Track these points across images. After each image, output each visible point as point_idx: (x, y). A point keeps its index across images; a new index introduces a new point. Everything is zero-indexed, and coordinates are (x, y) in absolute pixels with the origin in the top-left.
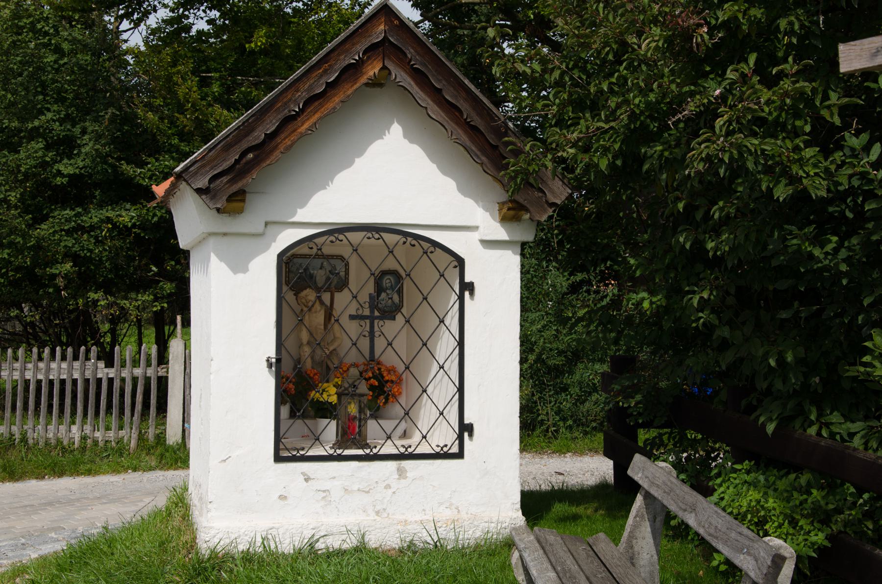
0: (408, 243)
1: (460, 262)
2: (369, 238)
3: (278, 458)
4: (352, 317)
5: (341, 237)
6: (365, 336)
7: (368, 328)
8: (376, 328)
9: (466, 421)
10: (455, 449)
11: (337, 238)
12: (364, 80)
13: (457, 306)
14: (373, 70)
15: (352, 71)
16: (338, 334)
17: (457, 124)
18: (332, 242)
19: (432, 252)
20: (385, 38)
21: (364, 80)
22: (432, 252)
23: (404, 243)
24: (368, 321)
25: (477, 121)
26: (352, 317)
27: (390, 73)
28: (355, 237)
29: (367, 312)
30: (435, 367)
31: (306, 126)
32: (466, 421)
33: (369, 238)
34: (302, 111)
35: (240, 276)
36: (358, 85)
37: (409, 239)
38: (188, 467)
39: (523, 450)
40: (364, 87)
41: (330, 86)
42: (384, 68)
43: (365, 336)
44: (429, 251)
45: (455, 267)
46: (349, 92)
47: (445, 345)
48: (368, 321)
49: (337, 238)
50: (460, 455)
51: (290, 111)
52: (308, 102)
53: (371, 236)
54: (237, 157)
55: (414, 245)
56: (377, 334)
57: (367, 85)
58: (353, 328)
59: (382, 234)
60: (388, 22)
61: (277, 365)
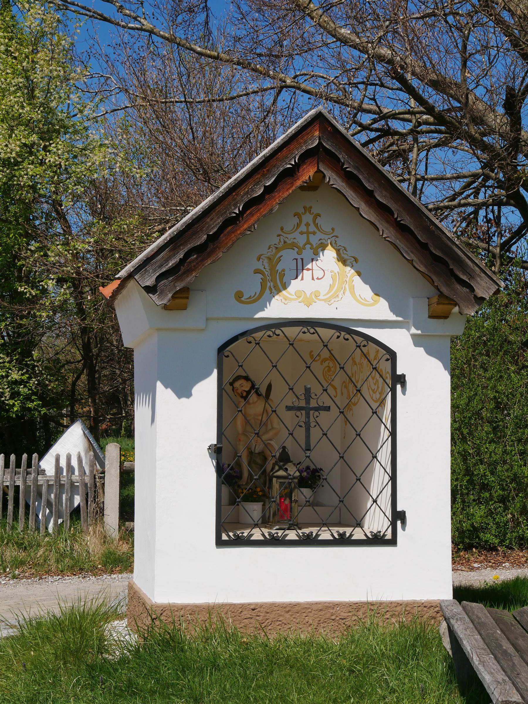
0: (342, 337)
1: (392, 356)
2: (304, 333)
3: (220, 543)
4: (289, 408)
5: (278, 332)
6: (301, 426)
7: (303, 419)
8: (312, 419)
9: (399, 509)
10: (389, 536)
11: (274, 333)
12: (299, 183)
13: (388, 490)
14: (308, 173)
15: (289, 174)
16: (276, 425)
17: (388, 222)
18: (269, 336)
19: (364, 346)
20: (320, 143)
21: (299, 183)
22: (364, 346)
23: (338, 337)
24: (303, 412)
25: (407, 221)
26: (289, 408)
27: (324, 176)
28: (292, 332)
29: (303, 404)
30: (370, 502)
31: (245, 226)
32: (399, 509)
33: (304, 333)
34: (242, 213)
35: (184, 400)
36: (294, 188)
37: (343, 333)
38: (132, 571)
39: (454, 562)
40: (299, 191)
41: (269, 190)
42: (319, 171)
43: (301, 426)
44: (362, 344)
45: (387, 360)
46: (286, 195)
47: (378, 479)
48: (303, 412)
49: (274, 333)
50: (393, 542)
51: (230, 213)
52: (248, 205)
53: (306, 331)
54: (181, 256)
55: (347, 339)
56: (312, 424)
57: (302, 188)
58: (289, 417)
59: (317, 329)
60: (323, 130)
61: (216, 451)
